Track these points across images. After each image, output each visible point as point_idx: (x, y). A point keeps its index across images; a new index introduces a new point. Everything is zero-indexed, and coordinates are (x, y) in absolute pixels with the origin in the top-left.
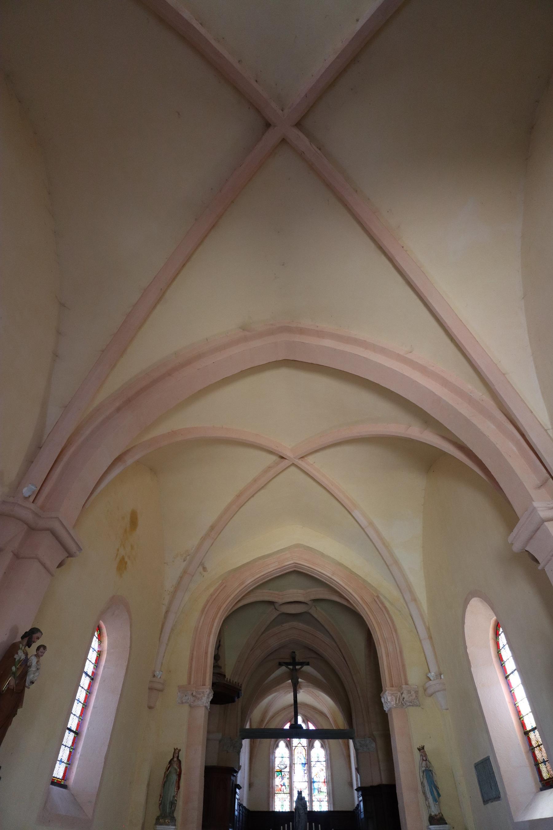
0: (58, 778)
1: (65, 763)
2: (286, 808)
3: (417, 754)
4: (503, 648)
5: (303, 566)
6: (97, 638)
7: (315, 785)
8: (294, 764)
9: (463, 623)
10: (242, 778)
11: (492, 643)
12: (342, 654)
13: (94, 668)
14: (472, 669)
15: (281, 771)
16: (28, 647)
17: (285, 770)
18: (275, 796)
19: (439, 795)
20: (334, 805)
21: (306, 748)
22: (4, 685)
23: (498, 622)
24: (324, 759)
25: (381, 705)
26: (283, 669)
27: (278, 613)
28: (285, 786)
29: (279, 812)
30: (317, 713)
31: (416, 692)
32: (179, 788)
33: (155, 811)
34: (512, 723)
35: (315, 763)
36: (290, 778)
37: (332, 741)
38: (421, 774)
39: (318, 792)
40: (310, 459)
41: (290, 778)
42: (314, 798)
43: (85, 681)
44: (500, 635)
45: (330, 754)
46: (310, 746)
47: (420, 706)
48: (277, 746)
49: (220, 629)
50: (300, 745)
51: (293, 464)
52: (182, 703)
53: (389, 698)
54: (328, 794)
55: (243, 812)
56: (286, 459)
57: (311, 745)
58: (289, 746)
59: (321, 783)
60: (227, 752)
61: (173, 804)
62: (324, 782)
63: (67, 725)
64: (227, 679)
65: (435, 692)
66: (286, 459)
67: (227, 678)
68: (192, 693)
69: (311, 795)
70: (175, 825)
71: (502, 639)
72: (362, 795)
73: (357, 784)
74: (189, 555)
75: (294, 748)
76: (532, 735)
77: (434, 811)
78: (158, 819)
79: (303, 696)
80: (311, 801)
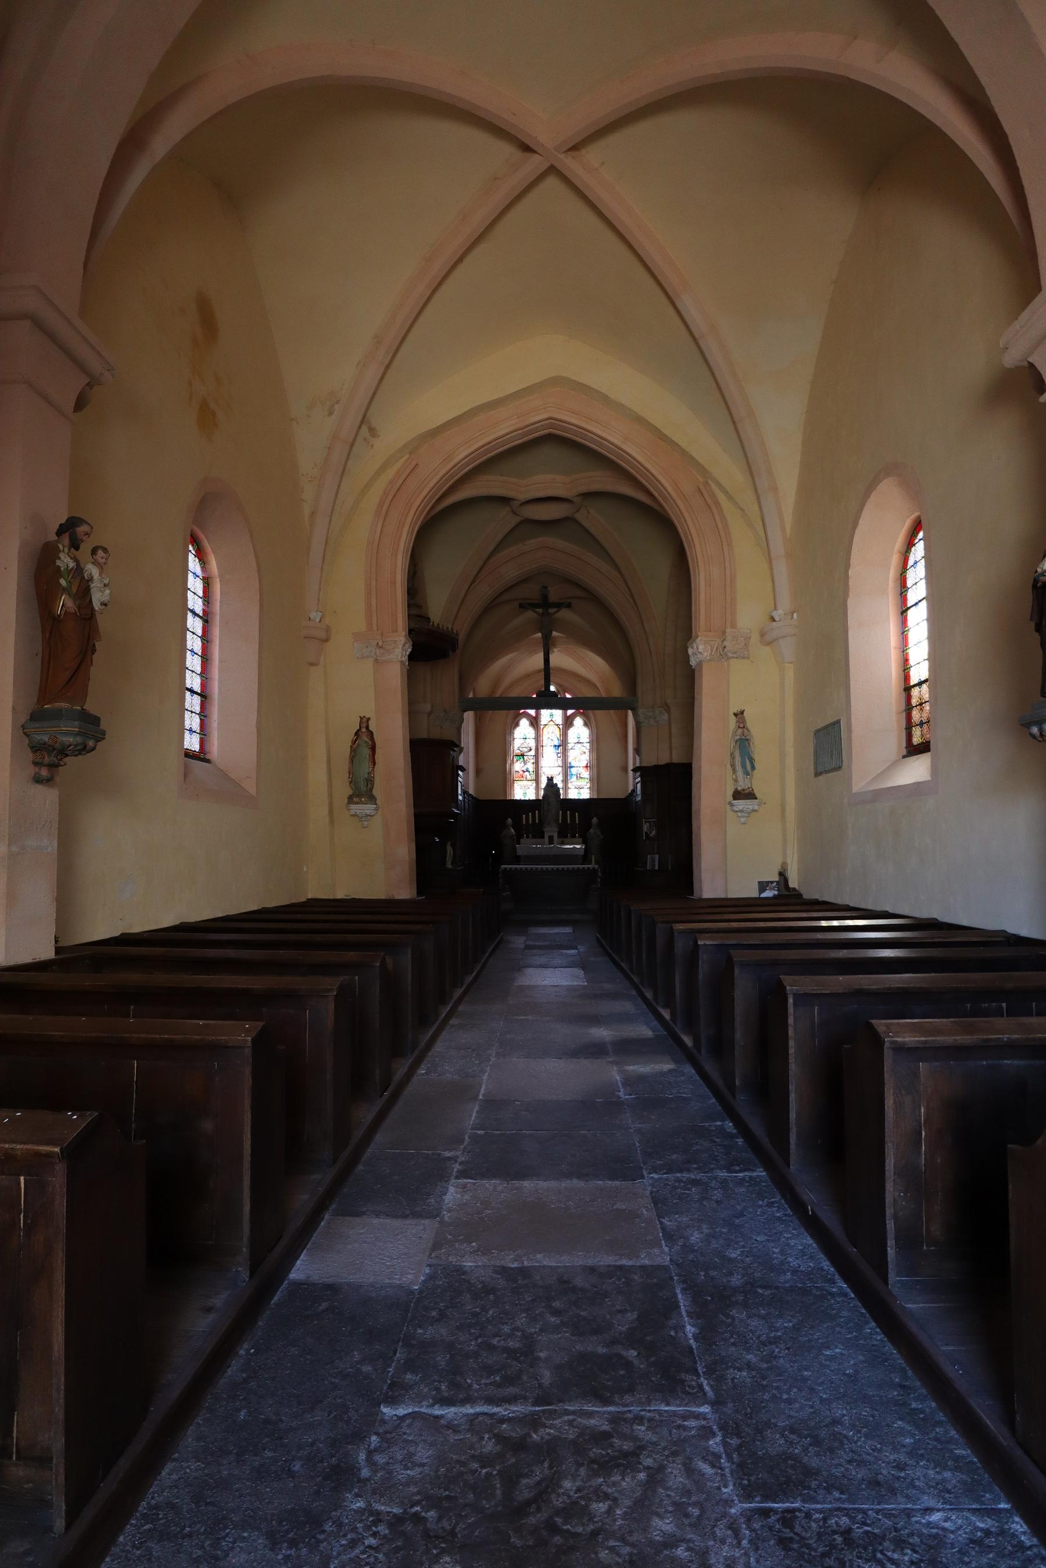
0: (195, 751)
1: (197, 733)
2: (531, 796)
3: (733, 721)
4: (912, 566)
5: (564, 424)
6: (195, 556)
7: (574, 771)
8: (542, 746)
9: (855, 524)
10: (467, 758)
11: (895, 560)
12: (630, 590)
13: (204, 604)
14: (850, 602)
15: (523, 755)
16: (74, 548)
17: (529, 753)
18: (514, 783)
19: (753, 768)
20: (598, 792)
21: (561, 727)
22: (57, 607)
23: (921, 521)
24: (588, 740)
25: (687, 657)
26: (530, 614)
27: (517, 520)
28: (529, 772)
29: (520, 801)
30: (579, 681)
31: (748, 639)
32: (374, 763)
33: (343, 790)
34: (891, 676)
35: (574, 744)
36: (537, 763)
37: (600, 713)
38: (733, 744)
39: (577, 777)
40: (593, 154)
41: (537, 763)
42: (570, 785)
43: (195, 624)
44: (914, 545)
45: (597, 734)
46: (568, 722)
47: (748, 658)
48: (517, 725)
49: (413, 547)
50: (551, 723)
51: (552, 170)
52: (363, 657)
53: (701, 648)
54: (591, 780)
55: (469, 801)
56: (535, 152)
57: (568, 723)
58: (535, 722)
59: (582, 768)
60: (441, 728)
61: (370, 781)
62: (587, 767)
63: (185, 684)
64: (433, 623)
65: (777, 639)
66: (535, 152)
67: (432, 621)
68: (378, 643)
69: (565, 781)
70: (376, 804)
71: (919, 550)
72: (641, 776)
73: (634, 763)
74: (338, 402)
75: (542, 727)
76: (915, 692)
77: (742, 785)
78: (350, 798)
79: (557, 658)
80: (566, 788)
